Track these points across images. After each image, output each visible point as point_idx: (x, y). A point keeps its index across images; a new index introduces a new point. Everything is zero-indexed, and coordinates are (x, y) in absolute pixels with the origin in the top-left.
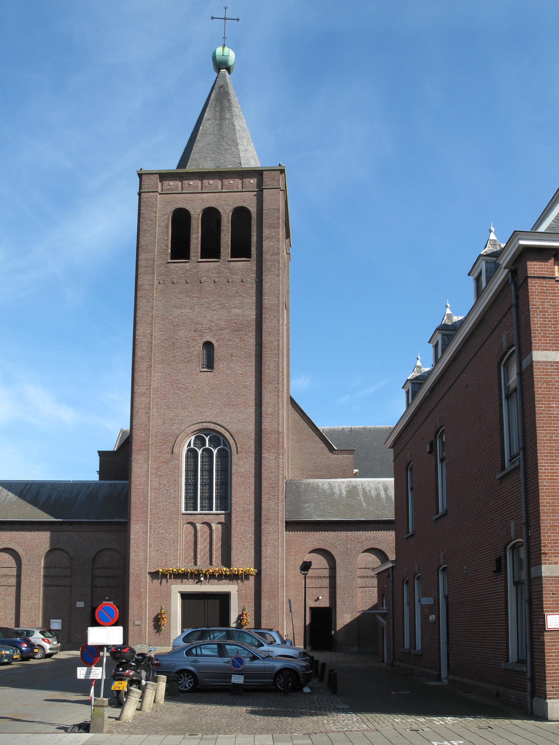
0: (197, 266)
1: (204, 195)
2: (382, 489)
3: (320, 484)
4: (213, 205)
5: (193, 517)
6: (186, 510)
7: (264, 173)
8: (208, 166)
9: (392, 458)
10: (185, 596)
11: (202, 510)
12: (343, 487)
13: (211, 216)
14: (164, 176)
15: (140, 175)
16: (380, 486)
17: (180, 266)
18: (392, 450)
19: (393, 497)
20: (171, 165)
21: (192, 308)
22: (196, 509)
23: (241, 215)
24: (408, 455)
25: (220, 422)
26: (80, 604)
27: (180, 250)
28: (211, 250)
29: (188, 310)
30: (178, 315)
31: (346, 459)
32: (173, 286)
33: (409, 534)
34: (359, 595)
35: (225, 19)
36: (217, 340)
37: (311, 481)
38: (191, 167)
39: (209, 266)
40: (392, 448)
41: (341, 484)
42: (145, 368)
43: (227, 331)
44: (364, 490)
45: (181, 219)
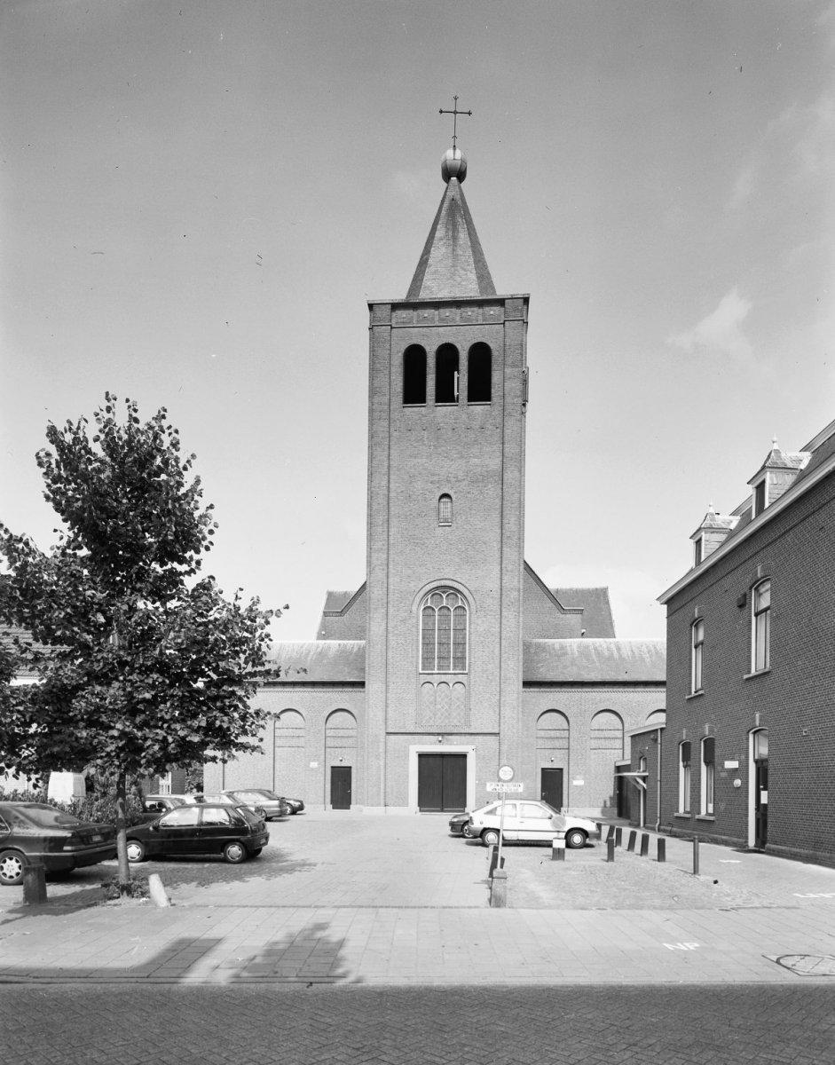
0: (433, 412)
1: (441, 329)
2: (614, 649)
3: (557, 646)
4: (450, 340)
5: (431, 676)
6: (423, 669)
7: (506, 301)
8: (444, 294)
9: (666, 615)
10: (421, 756)
11: (438, 669)
12: (575, 647)
13: (448, 354)
14: (395, 306)
15: (371, 306)
16: (613, 646)
17: (414, 411)
18: (666, 606)
19: (665, 653)
20: (400, 295)
21: (429, 457)
22: (449, 669)
23: (481, 354)
24: (696, 611)
25: (459, 580)
26: (314, 765)
27: (414, 394)
28: (445, 394)
29: (424, 460)
30: (414, 465)
31: (574, 619)
32: (409, 433)
33: (751, 675)
34: (593, 757)
35: (455, 112)
36: (455, 493)
37: (541, 640)
38: (424, 295)
39: (445, 410)
40: (666, 603)
41: (573, 643)
42: (381, 523)
43: (466, 482)
44: (596, 649)
45: (414, 356)
